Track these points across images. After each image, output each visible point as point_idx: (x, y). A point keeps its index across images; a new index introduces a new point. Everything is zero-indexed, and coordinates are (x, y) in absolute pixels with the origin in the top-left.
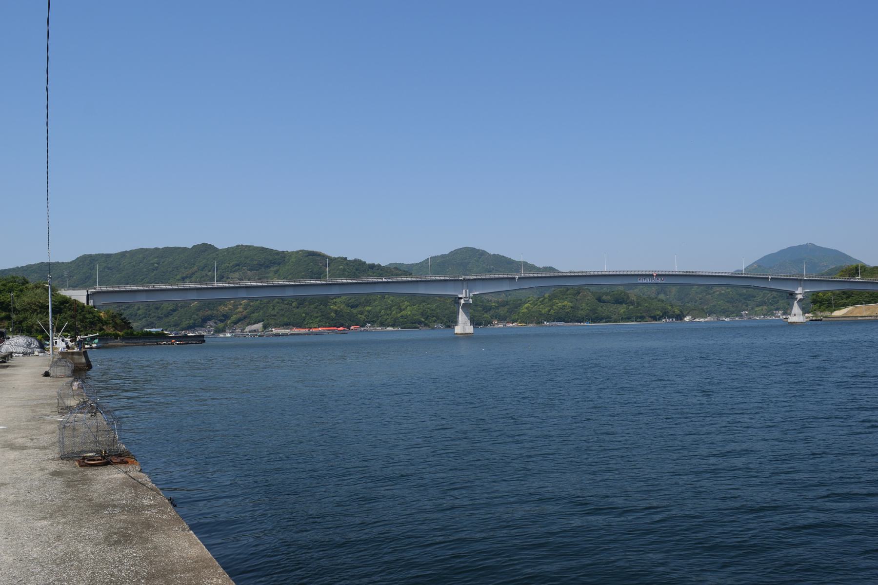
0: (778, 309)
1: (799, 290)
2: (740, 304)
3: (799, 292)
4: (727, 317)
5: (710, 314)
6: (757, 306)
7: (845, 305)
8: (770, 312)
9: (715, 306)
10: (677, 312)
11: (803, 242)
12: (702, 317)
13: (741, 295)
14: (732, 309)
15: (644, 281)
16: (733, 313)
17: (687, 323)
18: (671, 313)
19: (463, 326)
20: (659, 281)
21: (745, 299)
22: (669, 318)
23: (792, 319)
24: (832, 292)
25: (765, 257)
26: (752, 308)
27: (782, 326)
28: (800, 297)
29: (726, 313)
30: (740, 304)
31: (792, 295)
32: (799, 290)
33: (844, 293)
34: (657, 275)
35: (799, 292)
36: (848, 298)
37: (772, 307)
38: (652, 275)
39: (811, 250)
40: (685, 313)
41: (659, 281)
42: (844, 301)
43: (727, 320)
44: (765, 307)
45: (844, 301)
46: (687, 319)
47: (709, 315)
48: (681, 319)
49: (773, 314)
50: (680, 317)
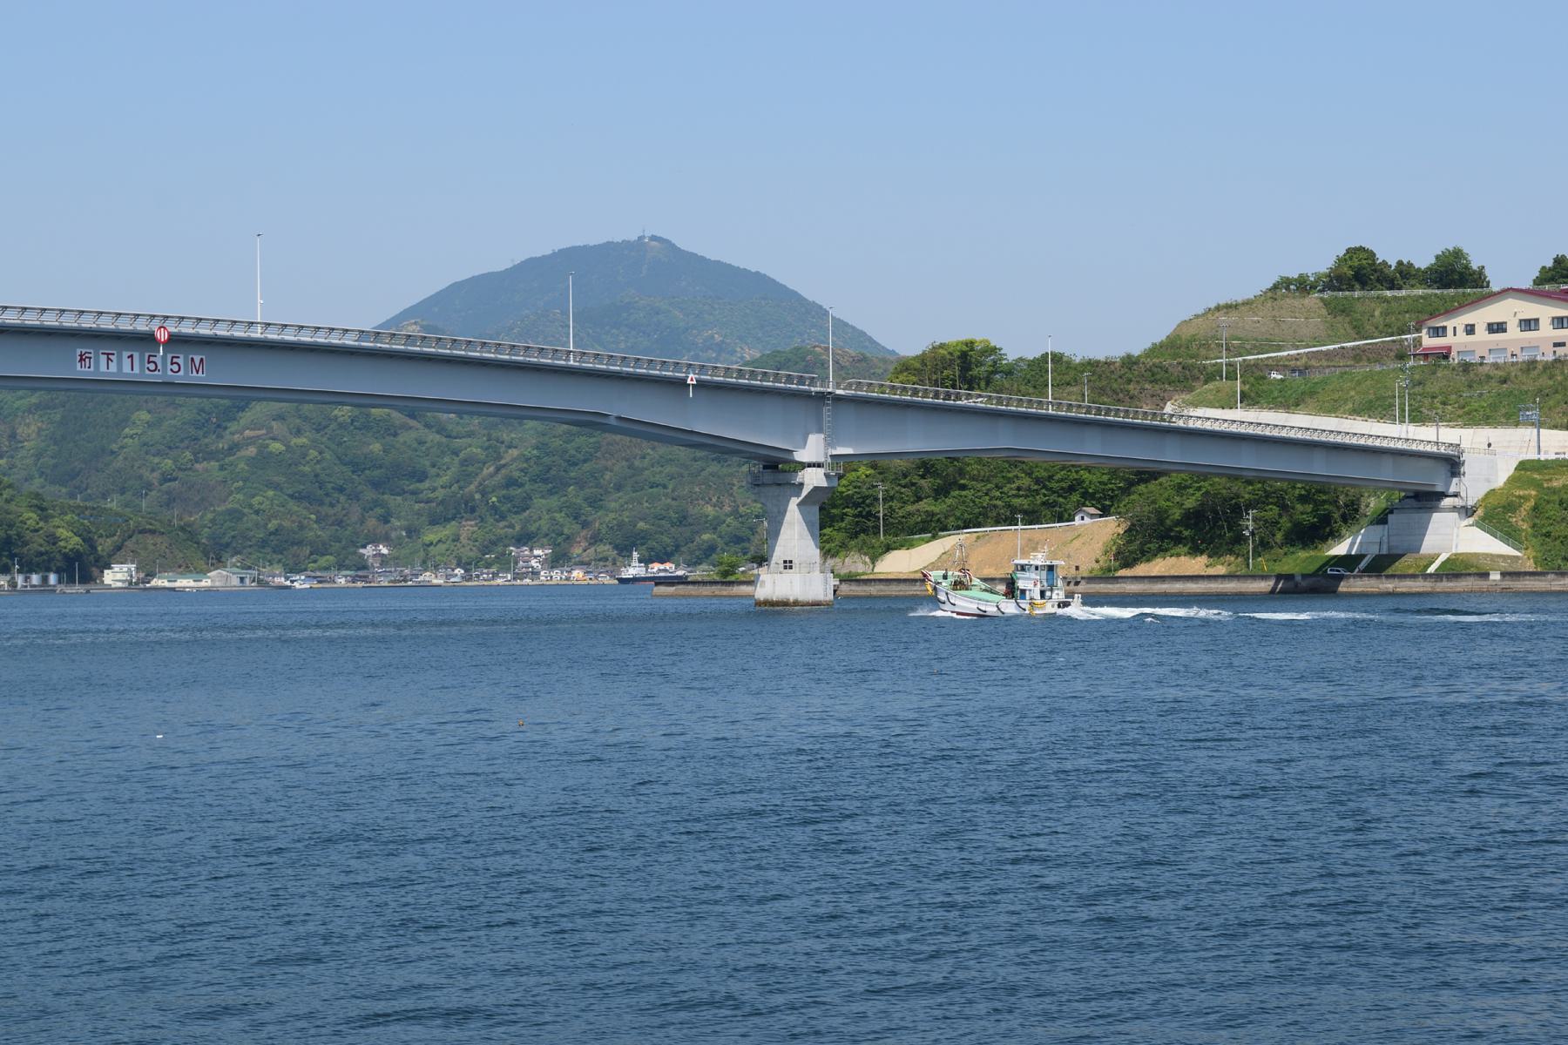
0: (525, 539)
1: (812, 449)
2: (356, 510)
3: (814, 453)
4: (293, 569)
5: (215, 555)
6: (434, 521)
7: (932, 527)
8: (492, 554)
9: (236, 515)
10: (70, 541)
11: (623, 231)
12: (186, 569)
13: (357, 466)
14: (315, 532)
15: (125, 366)
16: (319, 550)
17: (114, 594)
18: (37, 544)
19: (797, 569)
20: (182, 370)
21: (376, 485)
22: (27, 569)
23: (772, 585)
24: (874, 461)
25: (760, 280)
26: (412, 532)
27: (733, 616)
28: (813, 479)
29: (285, 548)
30: (356, 510)
31: (776, 469)
32: (812, 449)
33: (926, 466)
34: (176, 341)
35: (814, 453)
36: (941, 492)
37: (501, 529)
38: (147, 339)
39: (654, 265)
40: (104, 546)
41: (182, 370)
42: (926, 505)
43: (300, 583)
44: (468, 527)
45: (926, 505)
46: (116, 576)
47: (219, 562)
48: (87, 578)
49: (505, 563)
50: (81, 567)
